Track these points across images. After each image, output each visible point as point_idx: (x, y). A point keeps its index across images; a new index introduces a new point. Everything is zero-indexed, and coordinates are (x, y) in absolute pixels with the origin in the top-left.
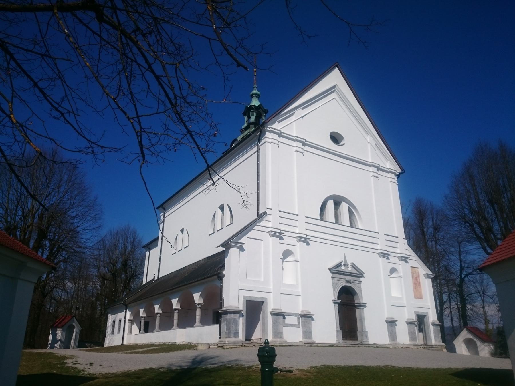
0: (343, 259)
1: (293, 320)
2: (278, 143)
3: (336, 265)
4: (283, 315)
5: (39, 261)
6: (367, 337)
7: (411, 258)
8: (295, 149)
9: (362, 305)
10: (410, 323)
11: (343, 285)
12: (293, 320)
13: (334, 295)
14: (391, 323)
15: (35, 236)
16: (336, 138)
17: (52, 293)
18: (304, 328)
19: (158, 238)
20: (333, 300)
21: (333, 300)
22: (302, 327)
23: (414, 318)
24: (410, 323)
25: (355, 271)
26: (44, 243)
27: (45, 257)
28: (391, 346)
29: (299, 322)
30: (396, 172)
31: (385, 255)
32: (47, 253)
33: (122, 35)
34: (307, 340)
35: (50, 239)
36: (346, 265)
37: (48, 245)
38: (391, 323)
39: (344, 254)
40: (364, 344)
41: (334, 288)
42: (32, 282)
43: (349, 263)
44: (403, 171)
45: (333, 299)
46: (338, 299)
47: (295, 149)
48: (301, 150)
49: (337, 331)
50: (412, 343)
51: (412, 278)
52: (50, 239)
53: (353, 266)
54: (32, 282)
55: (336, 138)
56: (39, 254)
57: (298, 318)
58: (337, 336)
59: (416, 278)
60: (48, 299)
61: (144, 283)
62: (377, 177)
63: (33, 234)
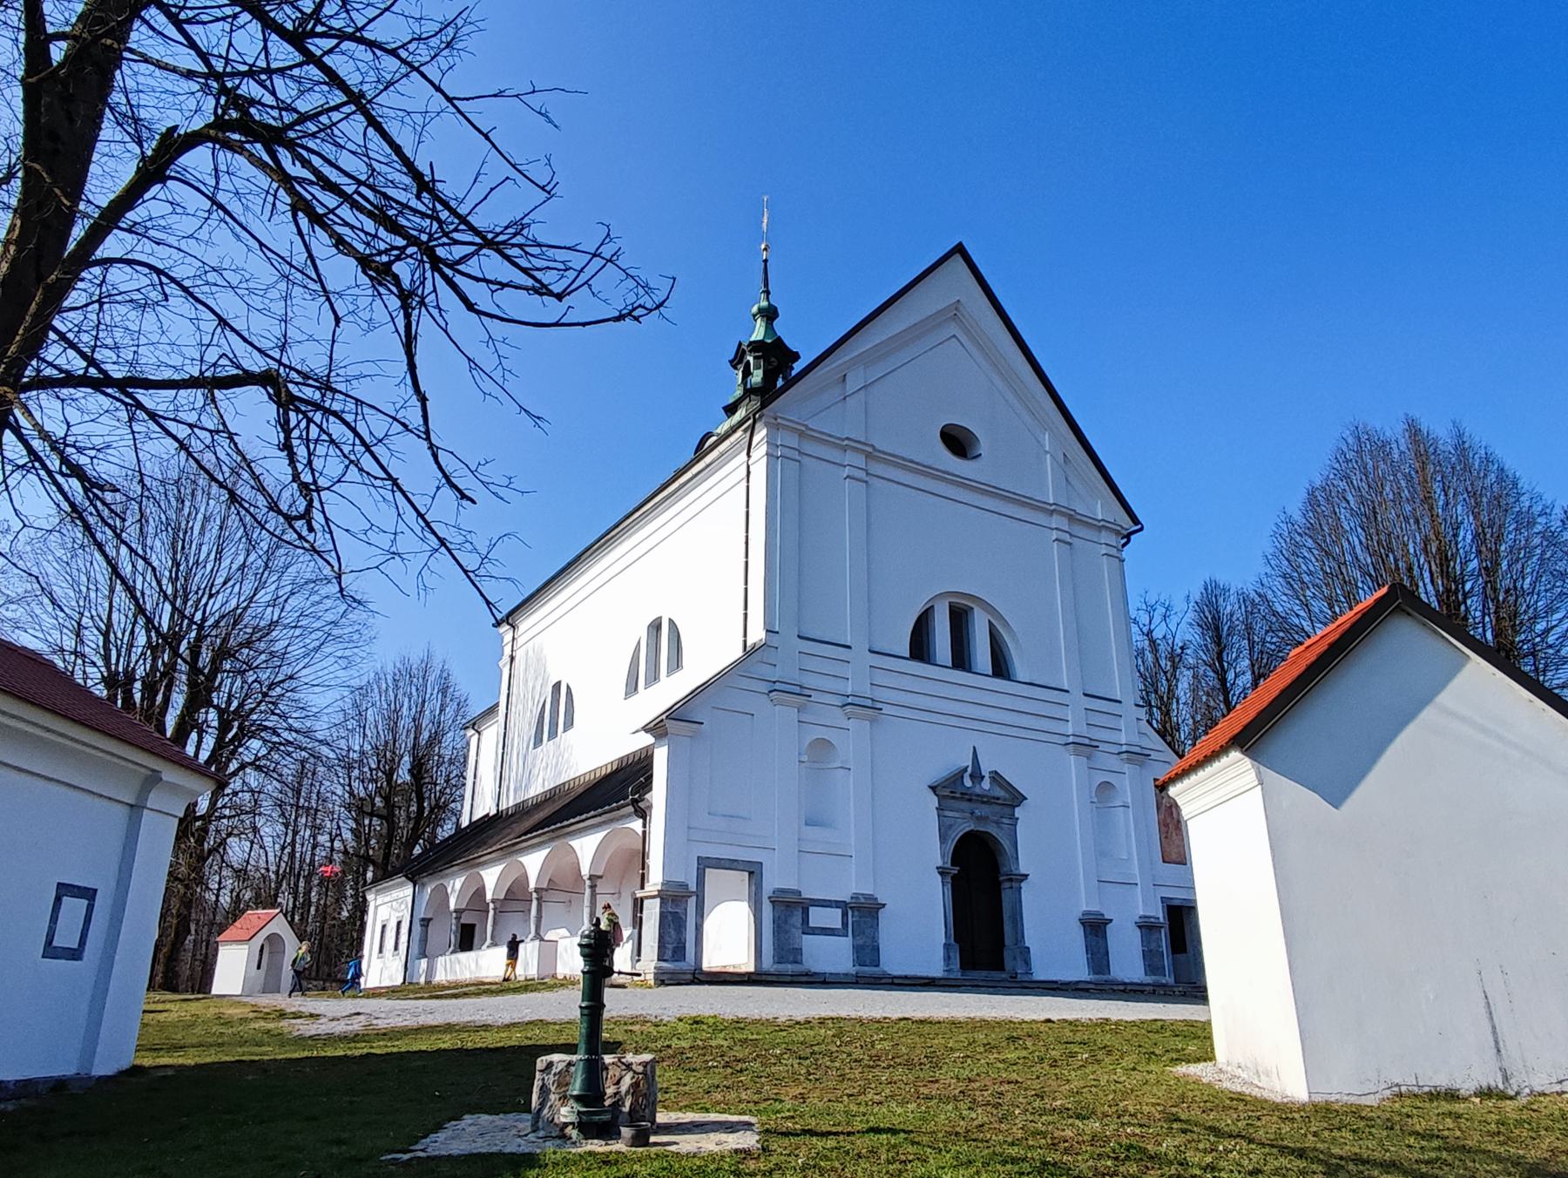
0: (968, 762)
1: (833, 918)
2: (866, 479)
3: (87, 730)
4: (805, 906)
5: (190, 765)
6: (1027, 962)
7: (1154, 755)
8: (1055, 535)
9: (942, 872)
10: (1147, 927)
11: (967, 829)
12: (833, 918)
13: (943, 856)
14: (1095, 927)
15: (178, 700)
16: (958, 442)
17: (225, 849)
18: (796, 946)
19: (497, 705)
20: (938, 868)
21: (938, 868)
22: (854, 937)
23: (1159, 913)
24: (1147, 927)
25: (1000, 793)
26: (202, 717)
27: (204, 755)
28: (1093, 986)
29: (845, 924)
30: (1119, 528)
31: (1085, 747)
32: (209, 742)
33: (1426, 601)
34: (866, 968)
35: (217, 707)
36: (977, 776)
37: (215, 724)
38: (1095, 927)
39: (974, 748)
40: (1018, 979)
41: (943, 838)
42: (176, 817)
43: (985, 772)
44: (1139, 526)
45: (940, 864)
46: (952, 865)
47: (1055, 535)
48: (862, 475)
49: (947, 946)
50: (1149, 979)
51: (1158, 809)
52: (217, 707)
53: (996, 777)
54: (176, 817)
55: (958, 442)
56: (190, 750)
57: (845, 915)
58: (947, 959)
60: (213, 862)
61: (465, 822)
62: (1070, 544)
63: (174, 695)
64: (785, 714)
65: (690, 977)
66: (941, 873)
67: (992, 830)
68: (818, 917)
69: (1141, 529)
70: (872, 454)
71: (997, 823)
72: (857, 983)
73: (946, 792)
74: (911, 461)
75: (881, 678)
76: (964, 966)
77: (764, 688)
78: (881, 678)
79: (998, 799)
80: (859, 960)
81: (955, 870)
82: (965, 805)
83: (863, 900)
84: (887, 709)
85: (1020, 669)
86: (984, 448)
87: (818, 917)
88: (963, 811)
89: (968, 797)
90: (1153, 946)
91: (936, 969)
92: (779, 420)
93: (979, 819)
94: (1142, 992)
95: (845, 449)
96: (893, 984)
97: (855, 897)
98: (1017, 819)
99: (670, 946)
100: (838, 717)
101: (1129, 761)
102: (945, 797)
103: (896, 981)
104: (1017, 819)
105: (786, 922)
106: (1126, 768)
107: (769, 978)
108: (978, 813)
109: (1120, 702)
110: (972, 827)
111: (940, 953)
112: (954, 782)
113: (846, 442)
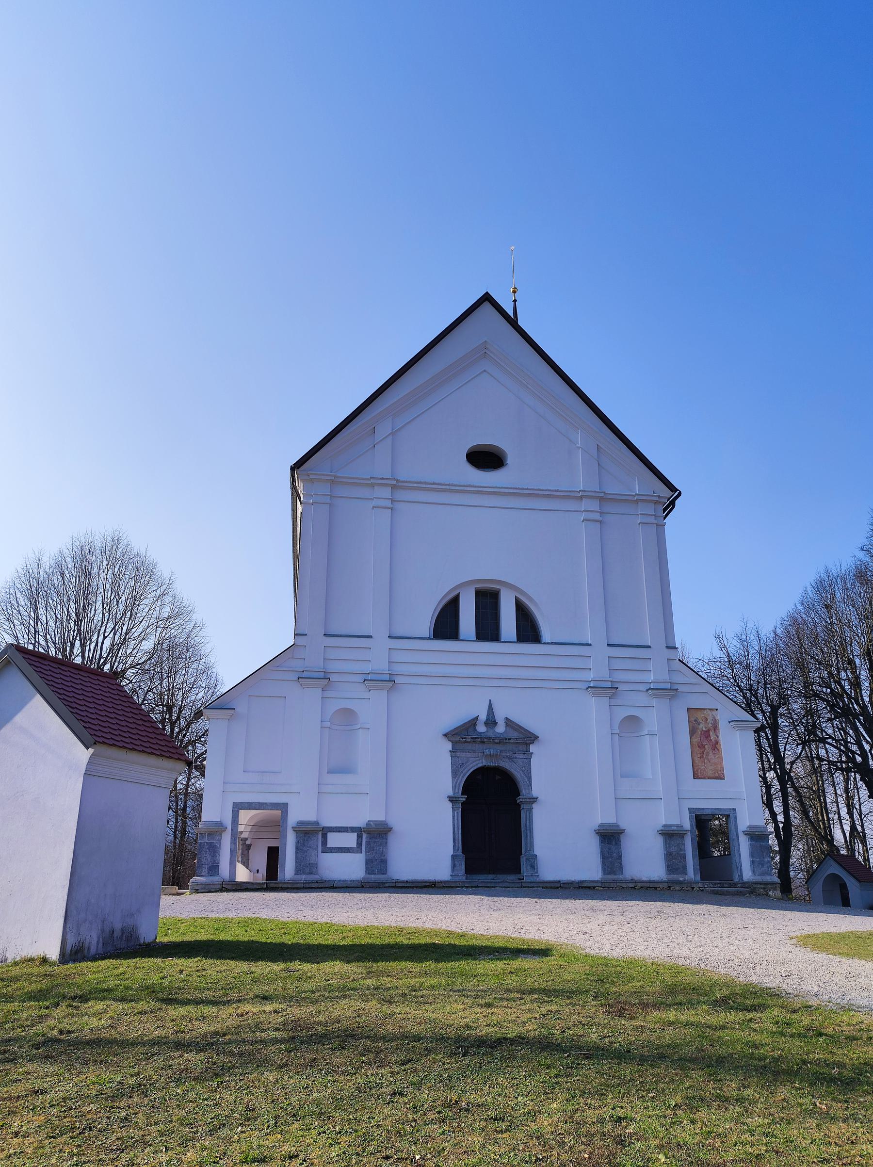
1: (350, 840)
4: (325, 831)
9: (452, 799)
11: (480, 765)
12: (350, 840)
13: (454, 787)
20: (449, 797)
21: (449, 797)
25: (513, 734)
29: (359, 844)
36: (491, 722)
41: (455, 774)
45: (451, 793)
46: (463, 794)
49: (453, 857)
53: (508, 722)
57: (360, 837)
58: (454, 866)
59: (706, 734)
64: (313, 695)
65: (219, 887)
66: (451, 801)
67: (505, 764)
68: (334, 840)
69: (680, 494)
70: (396, 485)
71: (510, 758)
72: (363, 887)
73: (457, 738)
74: (434, 483)
75: (618, 664)
76: (469, 870)
77: (360, 679)
78: (618, 664)
79: (510, 739)
80: (369, 869)
81: (464, 798)
82: (478, 747)
83: (374, 826)
84: (621, 687)
85: (546, 634)
86: (510, 460)
87: (334, 840)
88: (474, 751)
89: (482, 740)
90: (674, 850)
91: (443, 871)
92: (311, 476)
93: (490, 756)
94: (656, 888)
95: (373, 486)
96: (395, 887)
97: (368, 823)
98: (532, 753)
99: (206, 866)
100: (643, 699)
101: (656, 696)
102: (457, 742)
103: (397, 885)
104: (532, 753)
105: (303, 845)
106: (654, 702)
107: (285, 886)
108: (487, 752)
109: (590, 645)
110: (484, 764)
111: (447, 863)
112: (467, 730)
113: (372, 481)
